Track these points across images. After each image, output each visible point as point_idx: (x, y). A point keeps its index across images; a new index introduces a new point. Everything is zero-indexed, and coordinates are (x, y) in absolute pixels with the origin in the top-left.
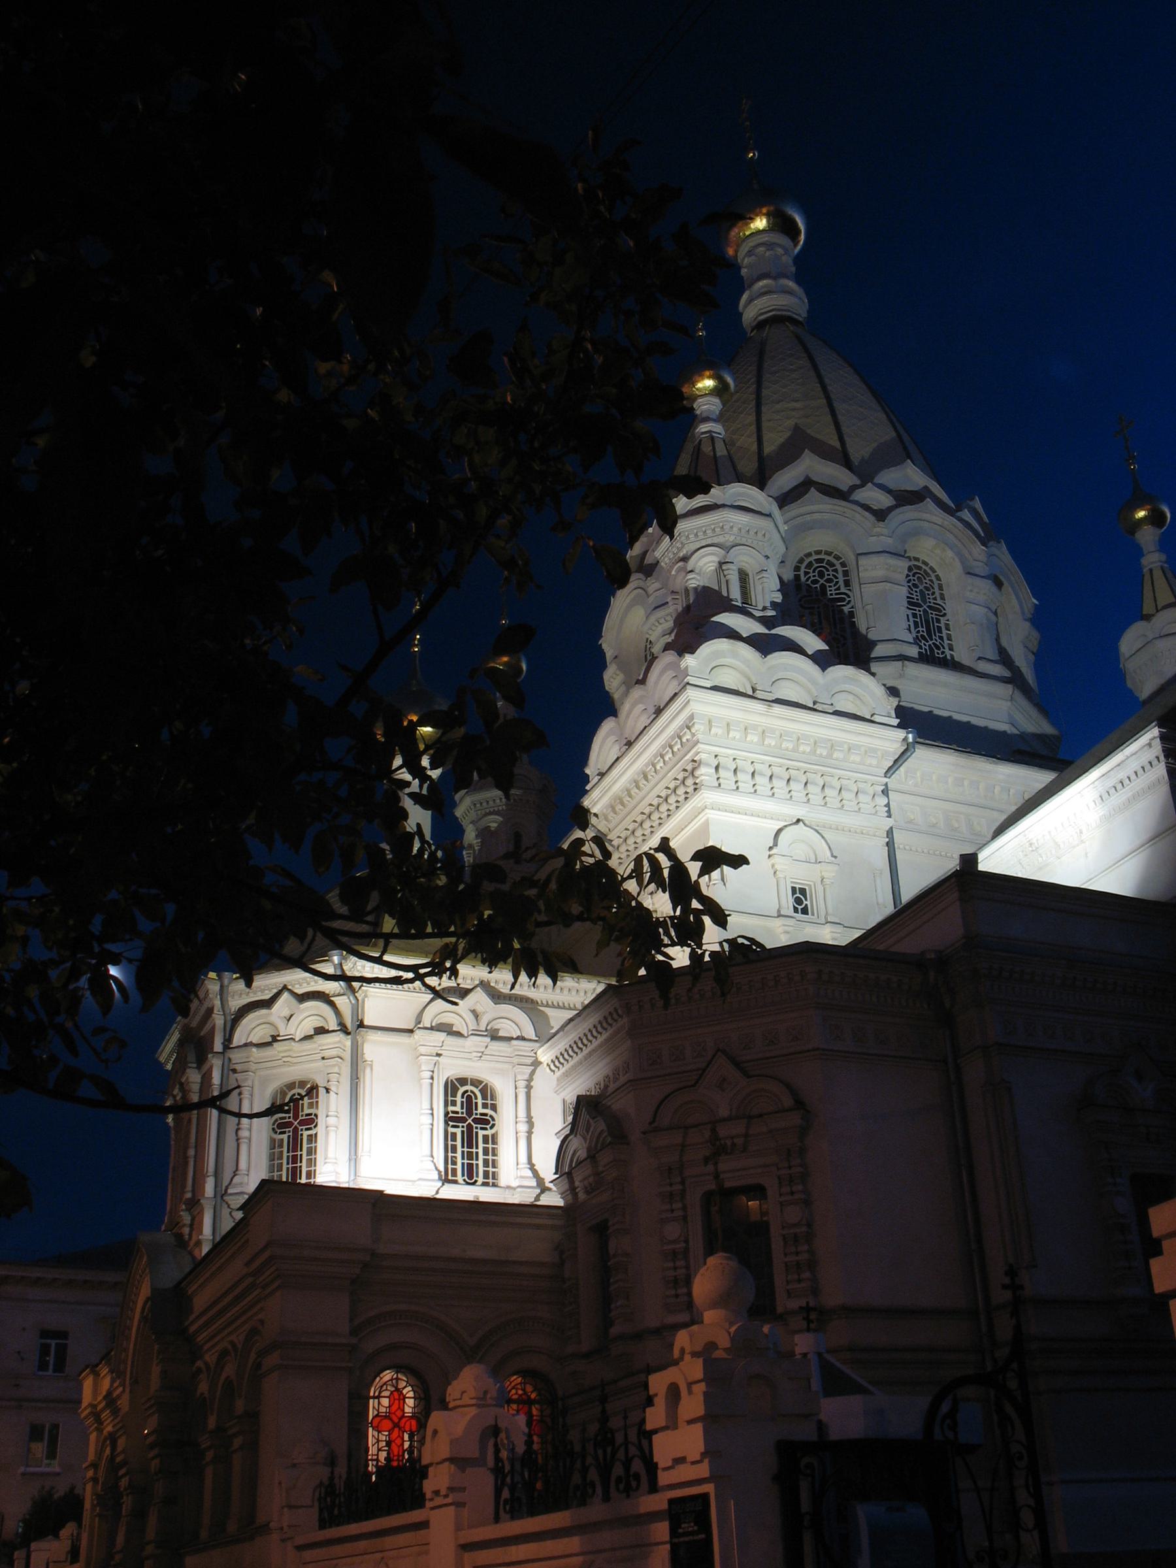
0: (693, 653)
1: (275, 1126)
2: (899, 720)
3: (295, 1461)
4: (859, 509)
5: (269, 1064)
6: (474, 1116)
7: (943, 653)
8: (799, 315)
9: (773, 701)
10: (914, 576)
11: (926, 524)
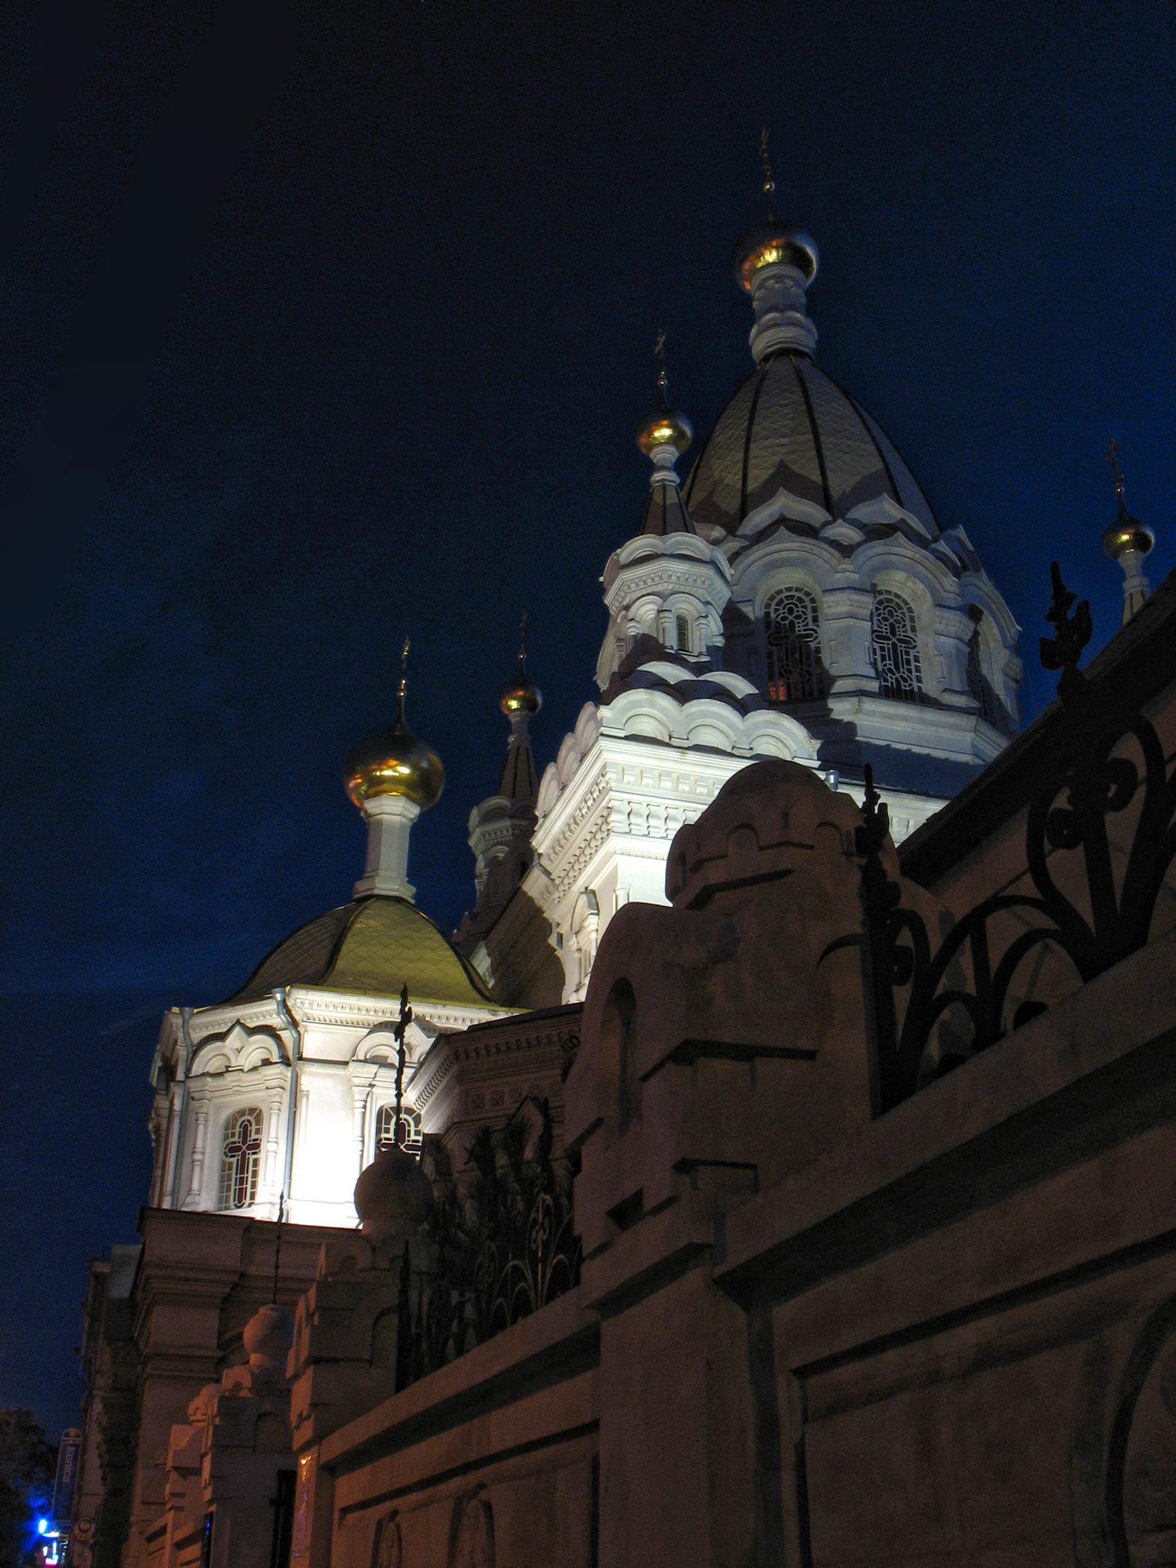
0: (608, 704)
1: (227, 1150)
2: (820, 762)
3: (158, 1462)
4: (825, 546)
5: (223, 1093)
6: (406, 1143)
7: (910, 685)
8: (806, 346)
9: (689, 748)
10: (884, 609)
11: (894, 558)
